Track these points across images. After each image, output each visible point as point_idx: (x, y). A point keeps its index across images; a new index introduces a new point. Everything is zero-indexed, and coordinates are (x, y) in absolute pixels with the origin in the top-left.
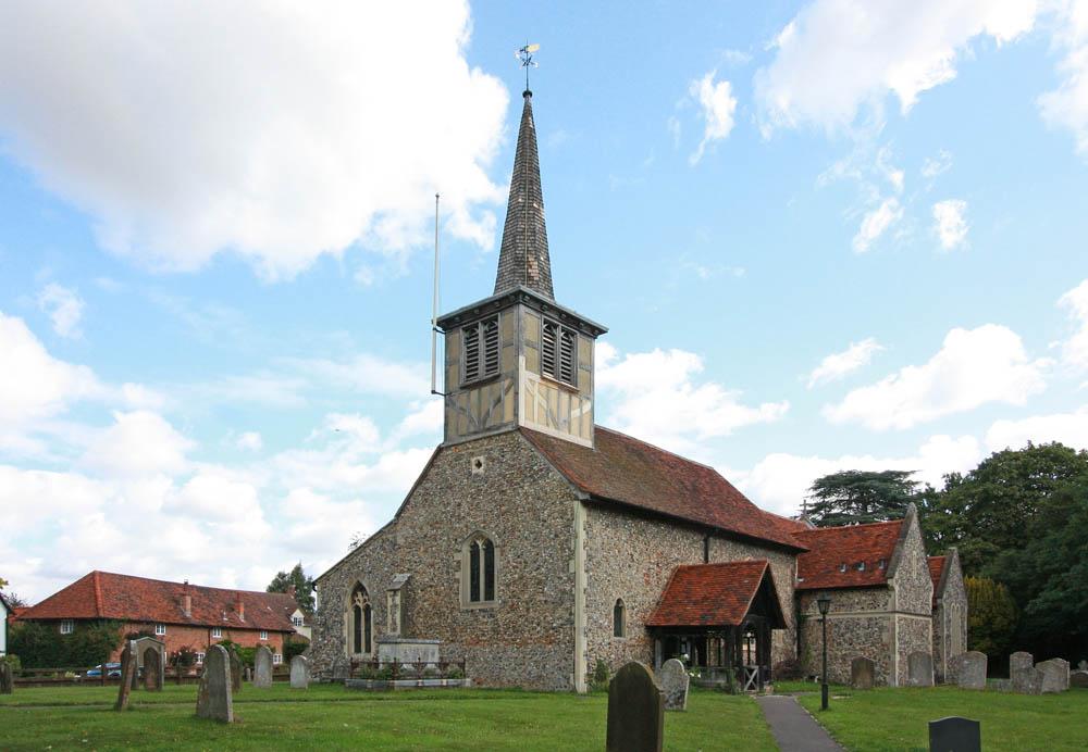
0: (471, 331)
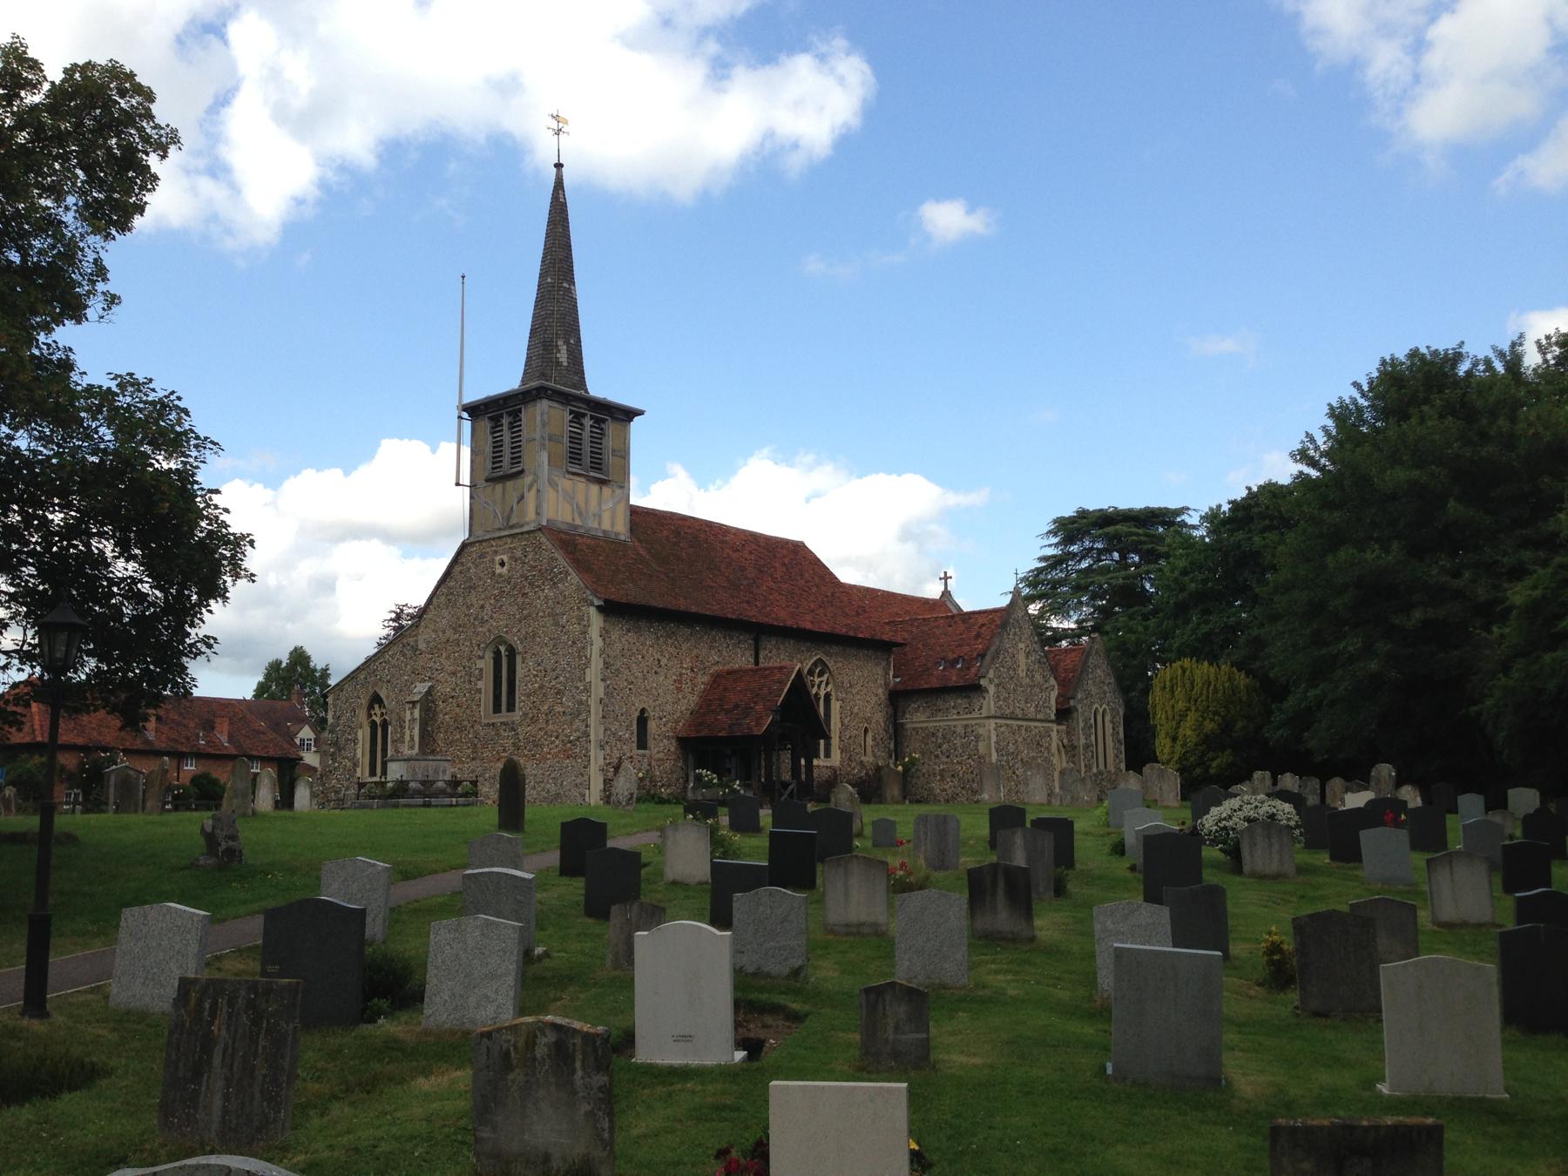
0: (496, 421)
